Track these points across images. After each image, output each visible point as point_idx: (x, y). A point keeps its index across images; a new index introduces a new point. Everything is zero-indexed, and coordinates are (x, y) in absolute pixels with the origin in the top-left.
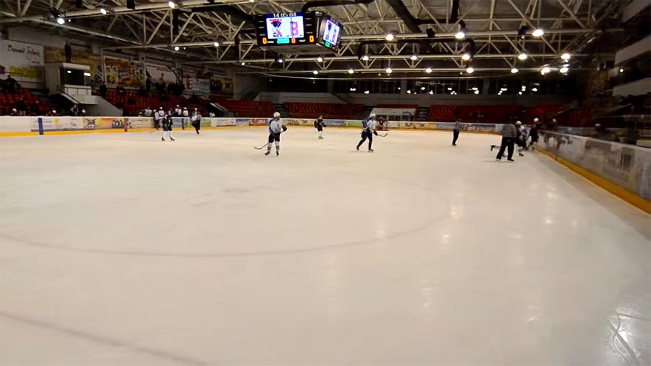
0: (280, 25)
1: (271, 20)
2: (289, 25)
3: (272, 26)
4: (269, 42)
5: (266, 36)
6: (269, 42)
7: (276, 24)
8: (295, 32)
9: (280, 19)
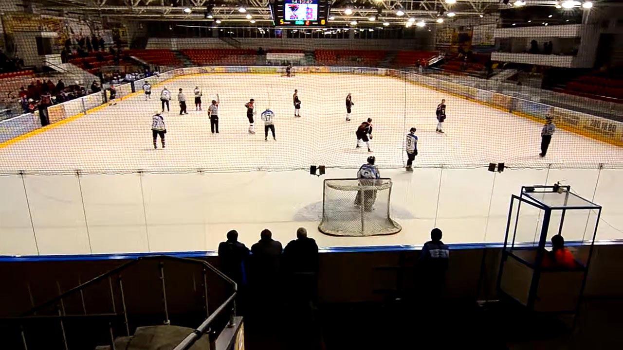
0: (297, 10)
1: (289, 5)
2: (305, 10)
3: (290, 10)
4: (285, 23)
5: (284, 18)
6: (285, 23)
7: (293, 9)
8: (309, 16)
9: (298, 4)
